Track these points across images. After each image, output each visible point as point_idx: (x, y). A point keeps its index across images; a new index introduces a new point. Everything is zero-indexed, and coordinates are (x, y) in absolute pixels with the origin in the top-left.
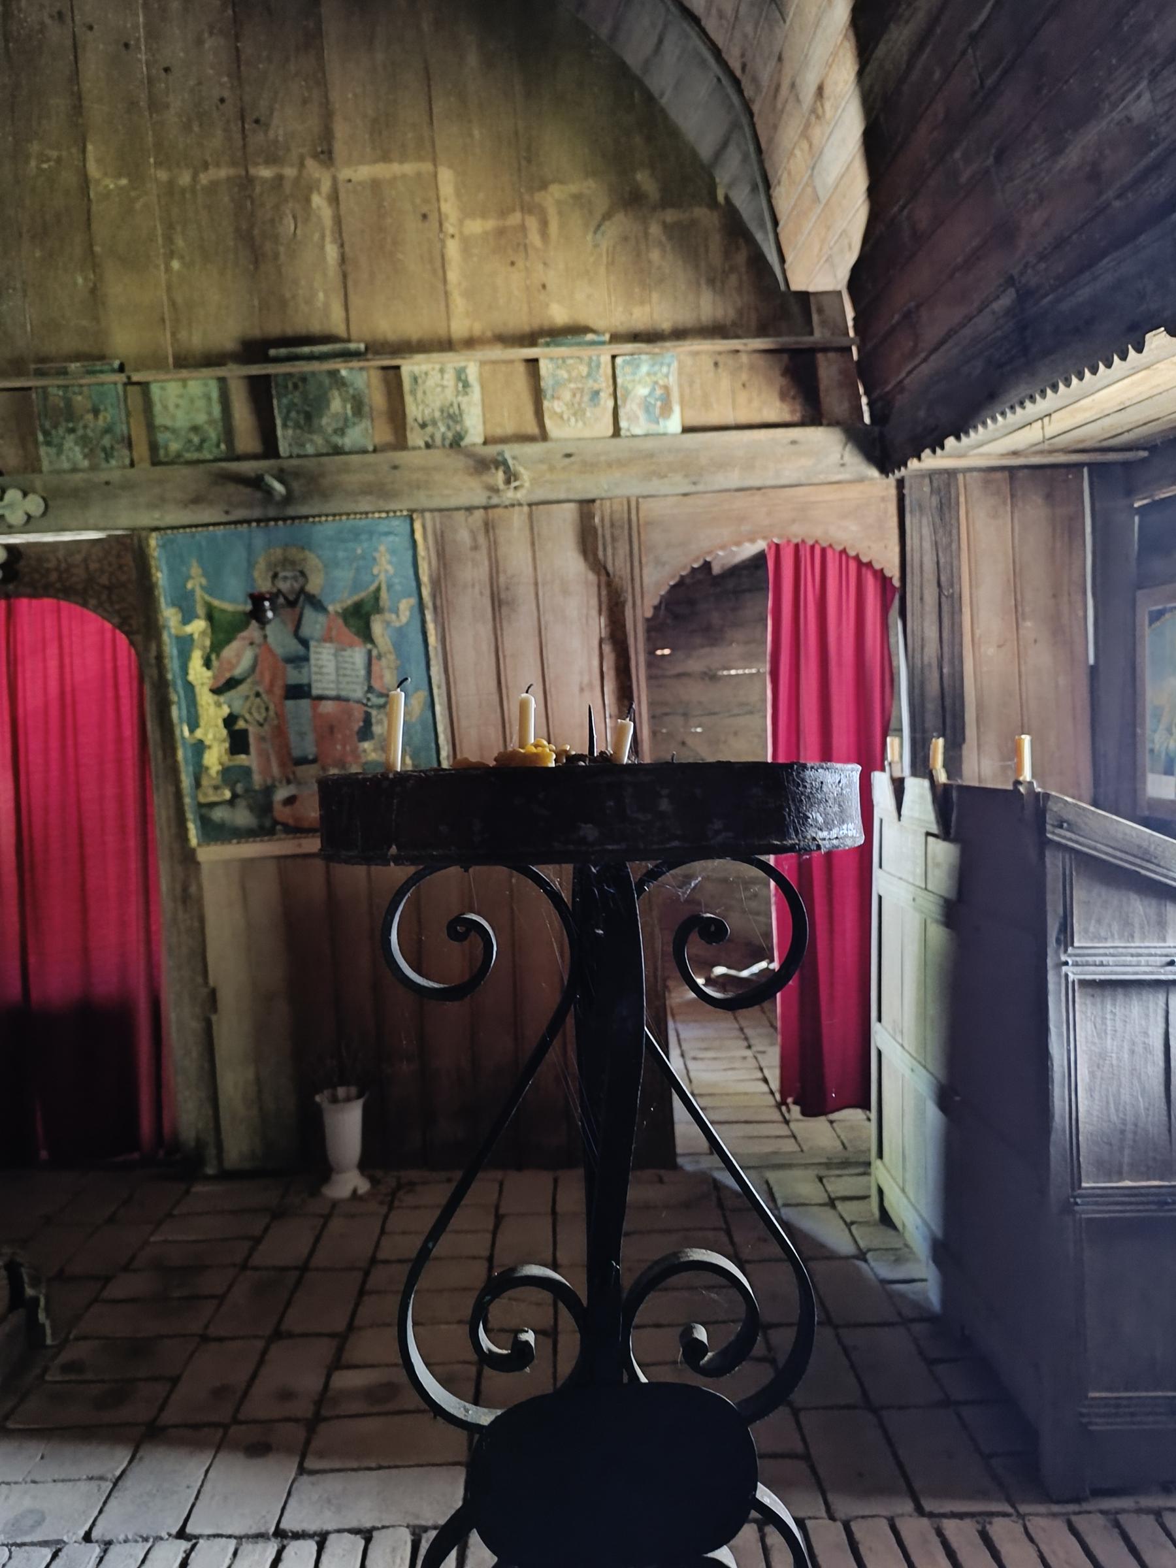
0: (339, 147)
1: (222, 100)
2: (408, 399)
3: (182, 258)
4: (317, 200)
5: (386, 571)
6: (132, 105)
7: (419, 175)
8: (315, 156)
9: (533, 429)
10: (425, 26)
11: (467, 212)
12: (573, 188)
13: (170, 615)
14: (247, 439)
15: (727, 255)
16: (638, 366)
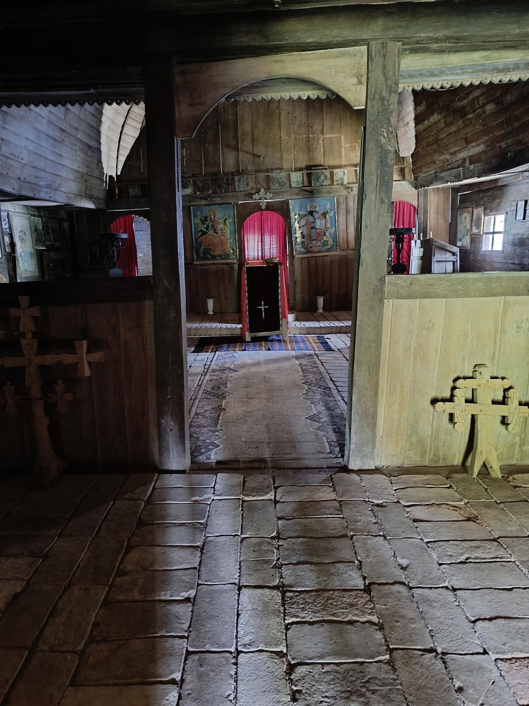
4: (320, 141)
11: (346, 143)
13: (292, 214)
14: (306, 184)
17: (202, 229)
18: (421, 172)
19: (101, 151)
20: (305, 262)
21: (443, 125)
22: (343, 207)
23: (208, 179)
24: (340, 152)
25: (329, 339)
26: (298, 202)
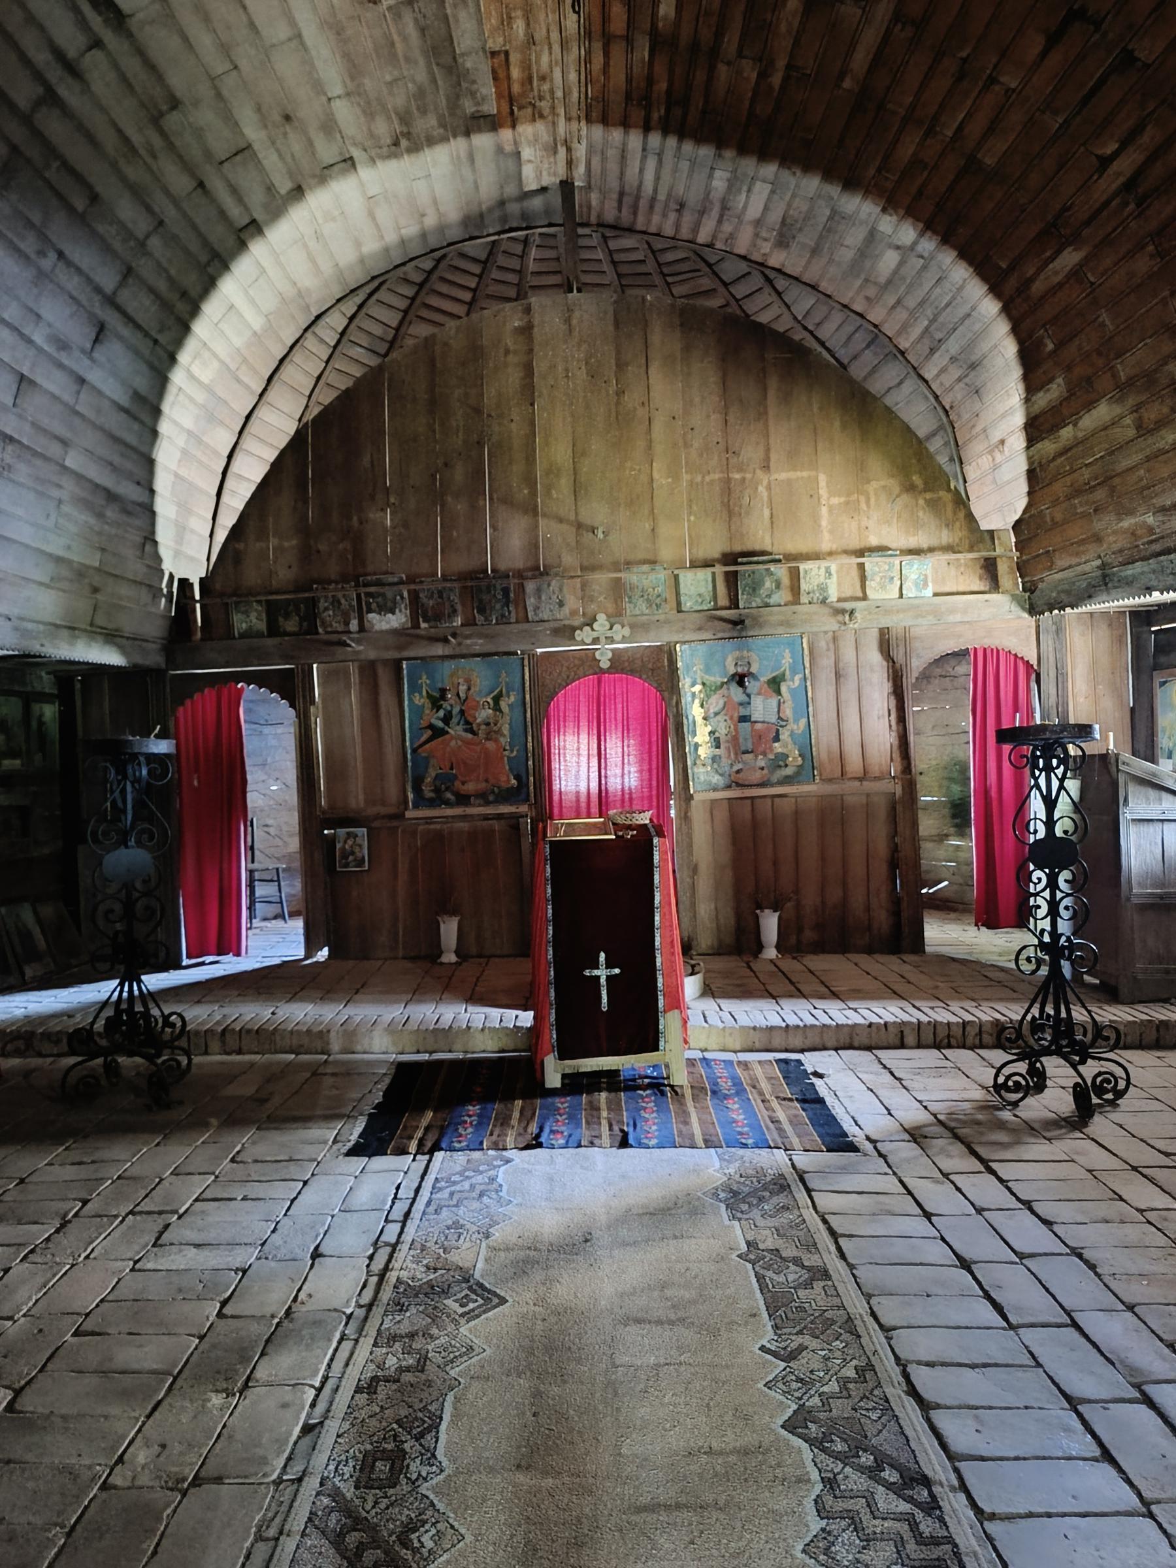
0: (772, 464)
2: (802, 581)
3: (695, 516)
4: (760, 488)
7: (809, 477)
9: (861, 595)
10: (815, 410)
11: (831, 494)
12: (883, 483)
13: (685, 683)
14: (723, 601)
15: (955, 513)
17: (434, 721)
18: (1050, 568)
19: (153, 514)
20: (722, 815)
21: (1132, 433)
22: (827, 662)
23: (451, 590)
24: (816, 518)
25: (821, 1076)
26: (702, 648)
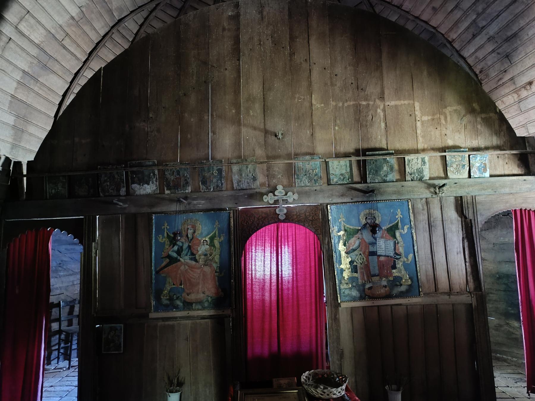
1: (352, 83)
5: (400, 217)
6: (326, 84)
8: (379, 99)
9: (442, 175)
11: (423, 114)
14: (356, 178)
15: (500, 126)
16: (477, 158)
